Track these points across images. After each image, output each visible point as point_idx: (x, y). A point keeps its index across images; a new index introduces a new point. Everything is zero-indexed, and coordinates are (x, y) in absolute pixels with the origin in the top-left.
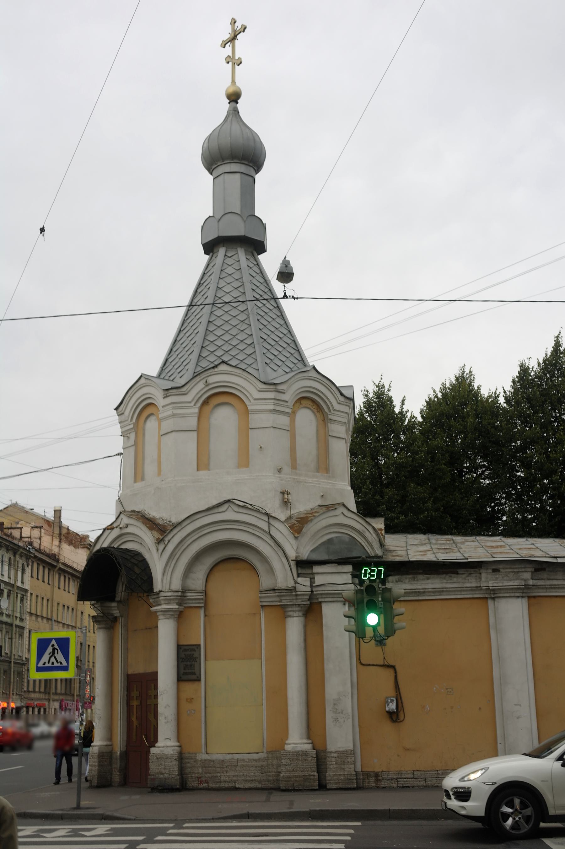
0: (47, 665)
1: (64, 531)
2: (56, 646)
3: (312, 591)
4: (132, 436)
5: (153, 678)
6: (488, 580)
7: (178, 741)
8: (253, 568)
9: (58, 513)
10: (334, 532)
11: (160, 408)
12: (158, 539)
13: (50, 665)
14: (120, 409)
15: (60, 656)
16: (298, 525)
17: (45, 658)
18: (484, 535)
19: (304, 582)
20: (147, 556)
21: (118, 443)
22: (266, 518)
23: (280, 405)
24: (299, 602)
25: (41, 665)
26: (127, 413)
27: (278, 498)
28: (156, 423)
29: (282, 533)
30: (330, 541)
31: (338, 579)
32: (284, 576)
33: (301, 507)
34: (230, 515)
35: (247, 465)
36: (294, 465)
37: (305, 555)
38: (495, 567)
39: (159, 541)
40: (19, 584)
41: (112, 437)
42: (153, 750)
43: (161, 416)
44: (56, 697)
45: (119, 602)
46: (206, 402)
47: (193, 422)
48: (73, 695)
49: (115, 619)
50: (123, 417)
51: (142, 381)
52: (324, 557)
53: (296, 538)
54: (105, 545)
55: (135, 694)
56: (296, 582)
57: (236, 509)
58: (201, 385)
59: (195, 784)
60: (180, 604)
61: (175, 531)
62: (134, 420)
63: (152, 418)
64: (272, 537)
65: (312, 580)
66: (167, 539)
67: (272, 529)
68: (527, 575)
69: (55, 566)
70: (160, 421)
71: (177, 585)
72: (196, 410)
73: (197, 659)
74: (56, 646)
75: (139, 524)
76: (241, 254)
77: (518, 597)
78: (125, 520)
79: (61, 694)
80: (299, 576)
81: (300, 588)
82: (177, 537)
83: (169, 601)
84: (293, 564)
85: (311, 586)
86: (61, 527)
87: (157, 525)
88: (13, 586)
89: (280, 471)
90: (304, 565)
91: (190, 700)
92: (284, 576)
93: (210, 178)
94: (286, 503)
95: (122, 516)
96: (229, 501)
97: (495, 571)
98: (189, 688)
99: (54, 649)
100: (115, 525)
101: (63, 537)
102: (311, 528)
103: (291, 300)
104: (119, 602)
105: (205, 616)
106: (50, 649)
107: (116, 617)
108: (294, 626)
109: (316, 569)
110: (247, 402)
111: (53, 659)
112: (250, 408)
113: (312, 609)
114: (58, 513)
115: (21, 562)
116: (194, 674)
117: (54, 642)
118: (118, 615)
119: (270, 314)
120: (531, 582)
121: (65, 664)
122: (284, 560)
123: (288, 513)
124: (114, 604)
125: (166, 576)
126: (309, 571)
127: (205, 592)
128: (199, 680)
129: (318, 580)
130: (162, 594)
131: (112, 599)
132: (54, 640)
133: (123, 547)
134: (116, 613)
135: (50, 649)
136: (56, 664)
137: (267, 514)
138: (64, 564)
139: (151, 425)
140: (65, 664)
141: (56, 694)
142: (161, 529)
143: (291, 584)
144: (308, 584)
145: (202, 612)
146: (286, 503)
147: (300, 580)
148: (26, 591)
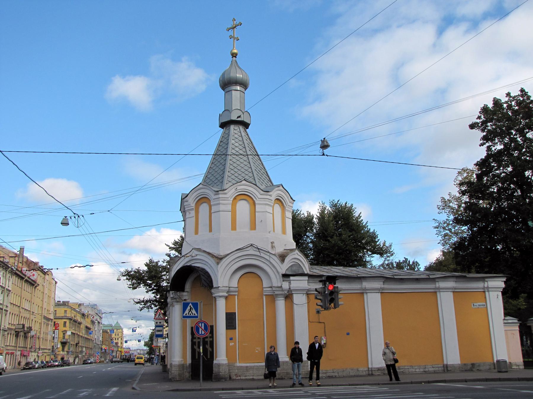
1: (25, 260)
2: (192, 307)
6: (366, 285)
9: (22, 250)
15: (194, 311)
17: (187, 312)
18: (350, 266)
25: (184, 315)
27: (270, 245)
29: (276, 261)
32: (277, 281)
34: (251, 251)
40: (7, 287)
44: (19, 349)
46: (235, 198)
47: (229, 208)
48: (27, 348)
57: (255, 249)
58: (234, 190)
59: (234, 377)
65: (290, 283)
69: (24, 278)
74: (192, 307)
76: (242, 128)
79: (22, 347)
86: (23, 256)
87: (215, 256)
88: (4, 288)
90: (286, 276)
92: (277, 281)
93: (223, 92)
94: (273, 247)
96: (252, 245)
99: (191, 308)
101: (24, 263)
102: (287, 260)
103: (325, 157)
106: (189, 308)
109: (292, 278)
110: (254, 199)
111: (190, 313)
112: (256, 202)
113: (289, 297)
115: (8, 275)
117: (190, 304)
121: (196, 315)
126: (288, 279)
132: (190, 304)
133: (193, 265)
135: (189, 308)
138: (29, 278)
140: (196, 315)
141: (19, 347)
148: (10, 291)
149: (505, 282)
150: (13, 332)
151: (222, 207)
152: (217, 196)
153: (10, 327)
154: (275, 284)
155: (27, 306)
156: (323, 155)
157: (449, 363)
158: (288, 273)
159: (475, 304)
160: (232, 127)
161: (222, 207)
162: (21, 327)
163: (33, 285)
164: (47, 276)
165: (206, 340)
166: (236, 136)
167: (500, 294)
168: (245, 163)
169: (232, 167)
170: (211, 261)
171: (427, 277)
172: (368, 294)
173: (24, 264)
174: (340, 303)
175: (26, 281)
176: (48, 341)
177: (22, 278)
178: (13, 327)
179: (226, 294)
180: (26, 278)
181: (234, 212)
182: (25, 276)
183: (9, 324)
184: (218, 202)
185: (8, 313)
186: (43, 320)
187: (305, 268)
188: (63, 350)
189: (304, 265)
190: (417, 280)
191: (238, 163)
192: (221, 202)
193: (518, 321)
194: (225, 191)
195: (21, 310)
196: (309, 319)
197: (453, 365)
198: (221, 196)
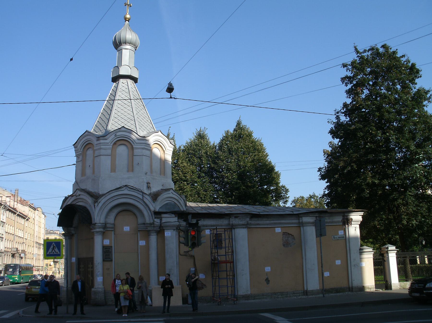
0: (51, 253)
2: (55, 245)
3: (161, 225)
4: (81, 157)
5: (91, 260)
6: (234, 221)
7: (103, 286)
8: (135, 215)
10: (108, 200)
11: (95, 145)
12: (95, 201)
13: (52, 253)
14: (75, 145)
15: (56, 250)
16: (155, 197)
17: (50, 250)
19: (157, 221)
20: (89, 208)
21: (74, 160)
22: (141, 194)
23: (147, 146)
24: (155, 229)
25: (48, 253)
26: (79, 147)
27: (145, 185)
28: (92, 151)
29: (148, 200)
30: (167, 204)
31: (173, 220)
32: (148, 218)
33: (155, 189)
34: (126, 192)
35: (133, 171)
36: (151, 172)
37: (157, 210)
38: (236, 216)
39: (95, 202)
41: (71, 157)
42: (93, 289)
43: (95, 148)
45: (74, 227)
46: (115, 144)
47: (109, 152)
49: (73, 235)
50: (77, 149)
51: (87, 133)
52: (165, 211)
53: (154, 202)
54: (69, 203)
55: (82, 266)
56: (154, 221)
57: (129, 189)
58: (113, 136)
60: (104, 229)
61: (102, 198)
62: (82, 150)
63: (90, 149)
64: (144, 202)
65: (161, 220)
66: (99, 201)
67: (144, 198)
68: (248, 219)
70: (94, 151)
71: (102, 221)
72: (111, 147)
73: (111, 252)
74: (55, 245)
75: (86, 194)
77: (244, 228)
78: (79, 193)
80: (155, 218)
81: (156, 223)
82: (102, 201)
83: (100, 228)
84: (153, 213)
85: (161, 223)
89: (146, 174)
90: (157, 214)
91: (108, 269)
92: (148, 218)
94: (149, 187)
95: (77, 191)
96: (126, 186)
97: (235, 217)
98: (107, 264)
99: (54, 247)
100: (74, 194)
102: (160, 198)
104: (74, 227)
105: (114, 234)
106: (52, 247)
107: (73, 234)
108: (153, 238)
109: (163, 215)
111: (53, 251)
112: (134, 147)
113: (160, 231)
114: (310, 195)
116: (110, 258)
117: (53, 244)
118: (74, 233)
119: (140, 107)
120: (250, 222)
122: (149, 211)
123: (150, 192)
124: (72, 228)
125: (99, 216)
127: (114, 224)
128: (112, 261)
129: (164, 220)
130: (96, 224)
131: (71, 226)
132: (53, 244)
134: (73, 232)
135: (52, 247)
136: (55, 253)
137: (142, 192)
138: (19, 212)
139: (90, 152)
140: (59, 253)
142: (96, 197)
143: (152, 221)
144: (159, 222)
145: (113, 232)
146: (149, 187)
147: (156, 220)
149: (363, 217)
150: (9, 254)
151: (103, 152)
152: (98, 142)
153: (6, 250)
154: (148, 221)
155: (20, 234)
156: (171, 98)
157: (308, 290)
158: (161, 210)
159: (335, 237)
160: (121, 80)
161: (103, 152)
162: (15, 250)
163: (25, 218)
164: (36, 211)
165: (182, 252)
166: (124, 89)
167: (358, 226)
168: (129, 112)
169: (116, 116)
170: (90, 200)
171: (292, 213)
172: (236, 229)
173: (19, 202)
174: (202, 241)
175: (18, 215)
176: (41, 260)
177: (15, 213)
178: (10, 250)
179: (102, 230)
180: (18, 213)
181: (113, 156)
182: (17, 211)
183: (5, 247)
184: (99, 147)
185: (4, 239)
186: (35, 245)
187: (182, 206)
188: (55, 267)
189: (179, 203)
190: (209, 226)
191: (122, 112)
192: (102, 147)
193: (373, 250)
194: (106, 137)
195: (15, 237)
196: (179, 253)
197: (312, 290)
198: (102, 141)
